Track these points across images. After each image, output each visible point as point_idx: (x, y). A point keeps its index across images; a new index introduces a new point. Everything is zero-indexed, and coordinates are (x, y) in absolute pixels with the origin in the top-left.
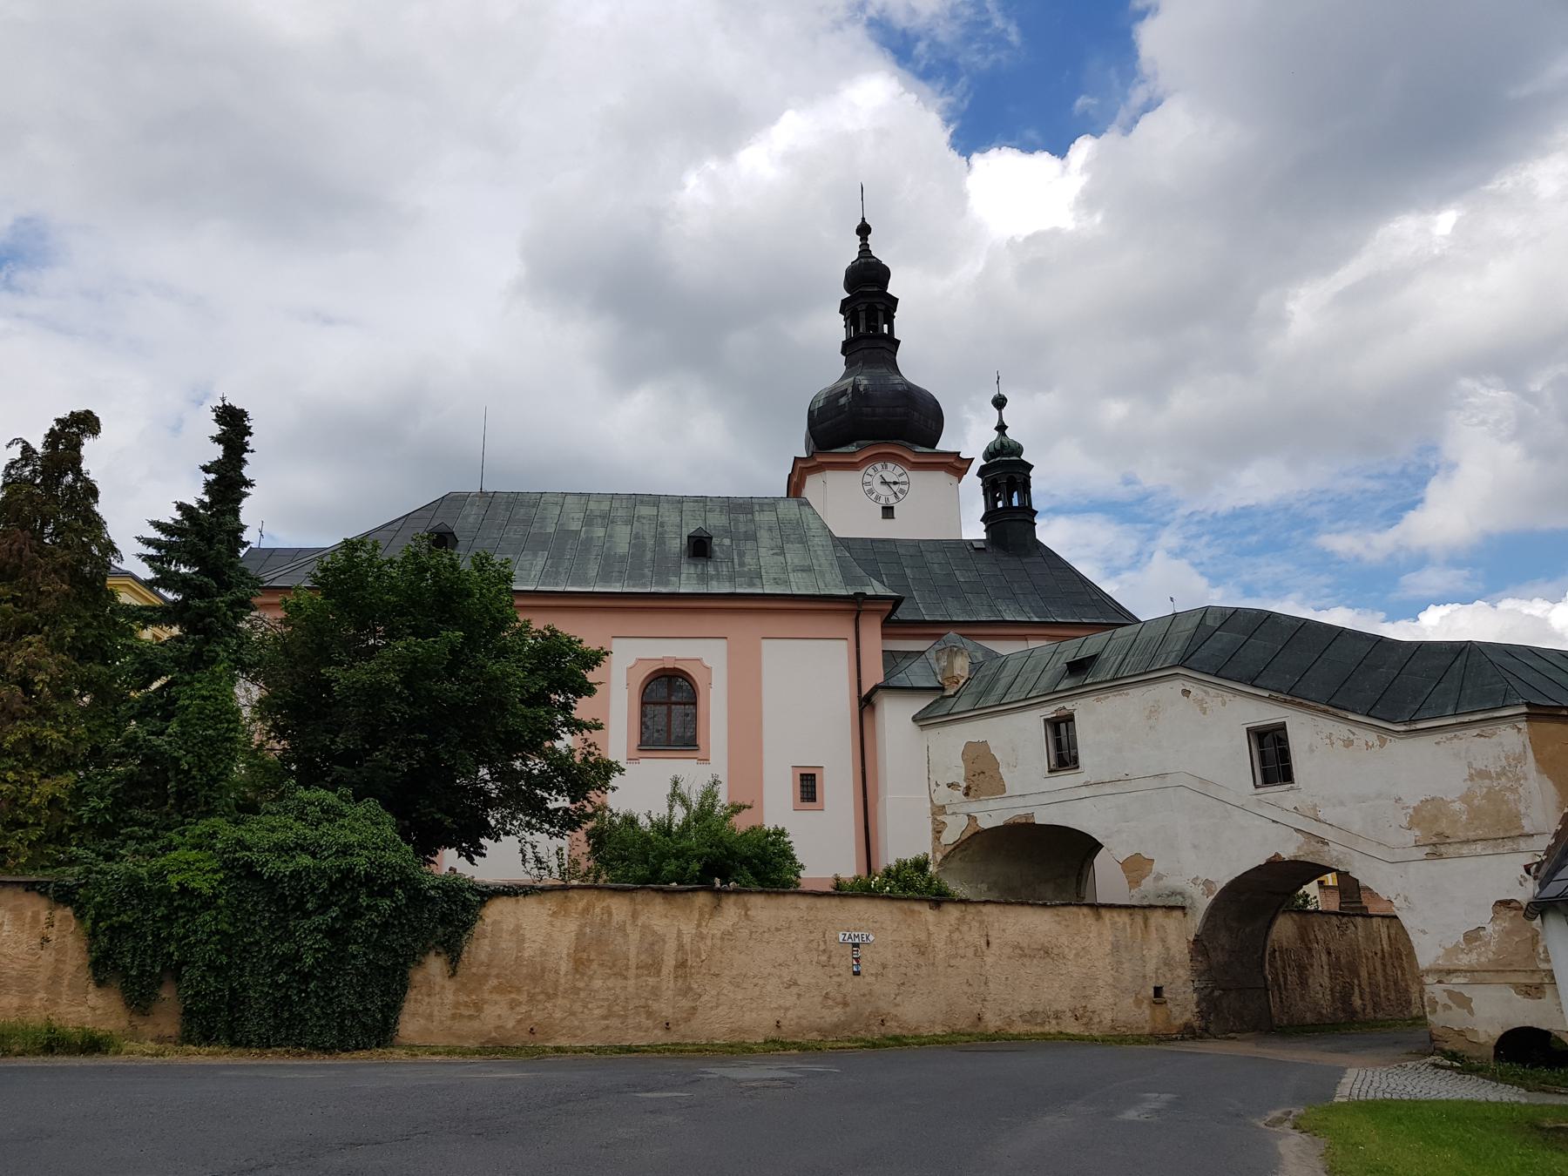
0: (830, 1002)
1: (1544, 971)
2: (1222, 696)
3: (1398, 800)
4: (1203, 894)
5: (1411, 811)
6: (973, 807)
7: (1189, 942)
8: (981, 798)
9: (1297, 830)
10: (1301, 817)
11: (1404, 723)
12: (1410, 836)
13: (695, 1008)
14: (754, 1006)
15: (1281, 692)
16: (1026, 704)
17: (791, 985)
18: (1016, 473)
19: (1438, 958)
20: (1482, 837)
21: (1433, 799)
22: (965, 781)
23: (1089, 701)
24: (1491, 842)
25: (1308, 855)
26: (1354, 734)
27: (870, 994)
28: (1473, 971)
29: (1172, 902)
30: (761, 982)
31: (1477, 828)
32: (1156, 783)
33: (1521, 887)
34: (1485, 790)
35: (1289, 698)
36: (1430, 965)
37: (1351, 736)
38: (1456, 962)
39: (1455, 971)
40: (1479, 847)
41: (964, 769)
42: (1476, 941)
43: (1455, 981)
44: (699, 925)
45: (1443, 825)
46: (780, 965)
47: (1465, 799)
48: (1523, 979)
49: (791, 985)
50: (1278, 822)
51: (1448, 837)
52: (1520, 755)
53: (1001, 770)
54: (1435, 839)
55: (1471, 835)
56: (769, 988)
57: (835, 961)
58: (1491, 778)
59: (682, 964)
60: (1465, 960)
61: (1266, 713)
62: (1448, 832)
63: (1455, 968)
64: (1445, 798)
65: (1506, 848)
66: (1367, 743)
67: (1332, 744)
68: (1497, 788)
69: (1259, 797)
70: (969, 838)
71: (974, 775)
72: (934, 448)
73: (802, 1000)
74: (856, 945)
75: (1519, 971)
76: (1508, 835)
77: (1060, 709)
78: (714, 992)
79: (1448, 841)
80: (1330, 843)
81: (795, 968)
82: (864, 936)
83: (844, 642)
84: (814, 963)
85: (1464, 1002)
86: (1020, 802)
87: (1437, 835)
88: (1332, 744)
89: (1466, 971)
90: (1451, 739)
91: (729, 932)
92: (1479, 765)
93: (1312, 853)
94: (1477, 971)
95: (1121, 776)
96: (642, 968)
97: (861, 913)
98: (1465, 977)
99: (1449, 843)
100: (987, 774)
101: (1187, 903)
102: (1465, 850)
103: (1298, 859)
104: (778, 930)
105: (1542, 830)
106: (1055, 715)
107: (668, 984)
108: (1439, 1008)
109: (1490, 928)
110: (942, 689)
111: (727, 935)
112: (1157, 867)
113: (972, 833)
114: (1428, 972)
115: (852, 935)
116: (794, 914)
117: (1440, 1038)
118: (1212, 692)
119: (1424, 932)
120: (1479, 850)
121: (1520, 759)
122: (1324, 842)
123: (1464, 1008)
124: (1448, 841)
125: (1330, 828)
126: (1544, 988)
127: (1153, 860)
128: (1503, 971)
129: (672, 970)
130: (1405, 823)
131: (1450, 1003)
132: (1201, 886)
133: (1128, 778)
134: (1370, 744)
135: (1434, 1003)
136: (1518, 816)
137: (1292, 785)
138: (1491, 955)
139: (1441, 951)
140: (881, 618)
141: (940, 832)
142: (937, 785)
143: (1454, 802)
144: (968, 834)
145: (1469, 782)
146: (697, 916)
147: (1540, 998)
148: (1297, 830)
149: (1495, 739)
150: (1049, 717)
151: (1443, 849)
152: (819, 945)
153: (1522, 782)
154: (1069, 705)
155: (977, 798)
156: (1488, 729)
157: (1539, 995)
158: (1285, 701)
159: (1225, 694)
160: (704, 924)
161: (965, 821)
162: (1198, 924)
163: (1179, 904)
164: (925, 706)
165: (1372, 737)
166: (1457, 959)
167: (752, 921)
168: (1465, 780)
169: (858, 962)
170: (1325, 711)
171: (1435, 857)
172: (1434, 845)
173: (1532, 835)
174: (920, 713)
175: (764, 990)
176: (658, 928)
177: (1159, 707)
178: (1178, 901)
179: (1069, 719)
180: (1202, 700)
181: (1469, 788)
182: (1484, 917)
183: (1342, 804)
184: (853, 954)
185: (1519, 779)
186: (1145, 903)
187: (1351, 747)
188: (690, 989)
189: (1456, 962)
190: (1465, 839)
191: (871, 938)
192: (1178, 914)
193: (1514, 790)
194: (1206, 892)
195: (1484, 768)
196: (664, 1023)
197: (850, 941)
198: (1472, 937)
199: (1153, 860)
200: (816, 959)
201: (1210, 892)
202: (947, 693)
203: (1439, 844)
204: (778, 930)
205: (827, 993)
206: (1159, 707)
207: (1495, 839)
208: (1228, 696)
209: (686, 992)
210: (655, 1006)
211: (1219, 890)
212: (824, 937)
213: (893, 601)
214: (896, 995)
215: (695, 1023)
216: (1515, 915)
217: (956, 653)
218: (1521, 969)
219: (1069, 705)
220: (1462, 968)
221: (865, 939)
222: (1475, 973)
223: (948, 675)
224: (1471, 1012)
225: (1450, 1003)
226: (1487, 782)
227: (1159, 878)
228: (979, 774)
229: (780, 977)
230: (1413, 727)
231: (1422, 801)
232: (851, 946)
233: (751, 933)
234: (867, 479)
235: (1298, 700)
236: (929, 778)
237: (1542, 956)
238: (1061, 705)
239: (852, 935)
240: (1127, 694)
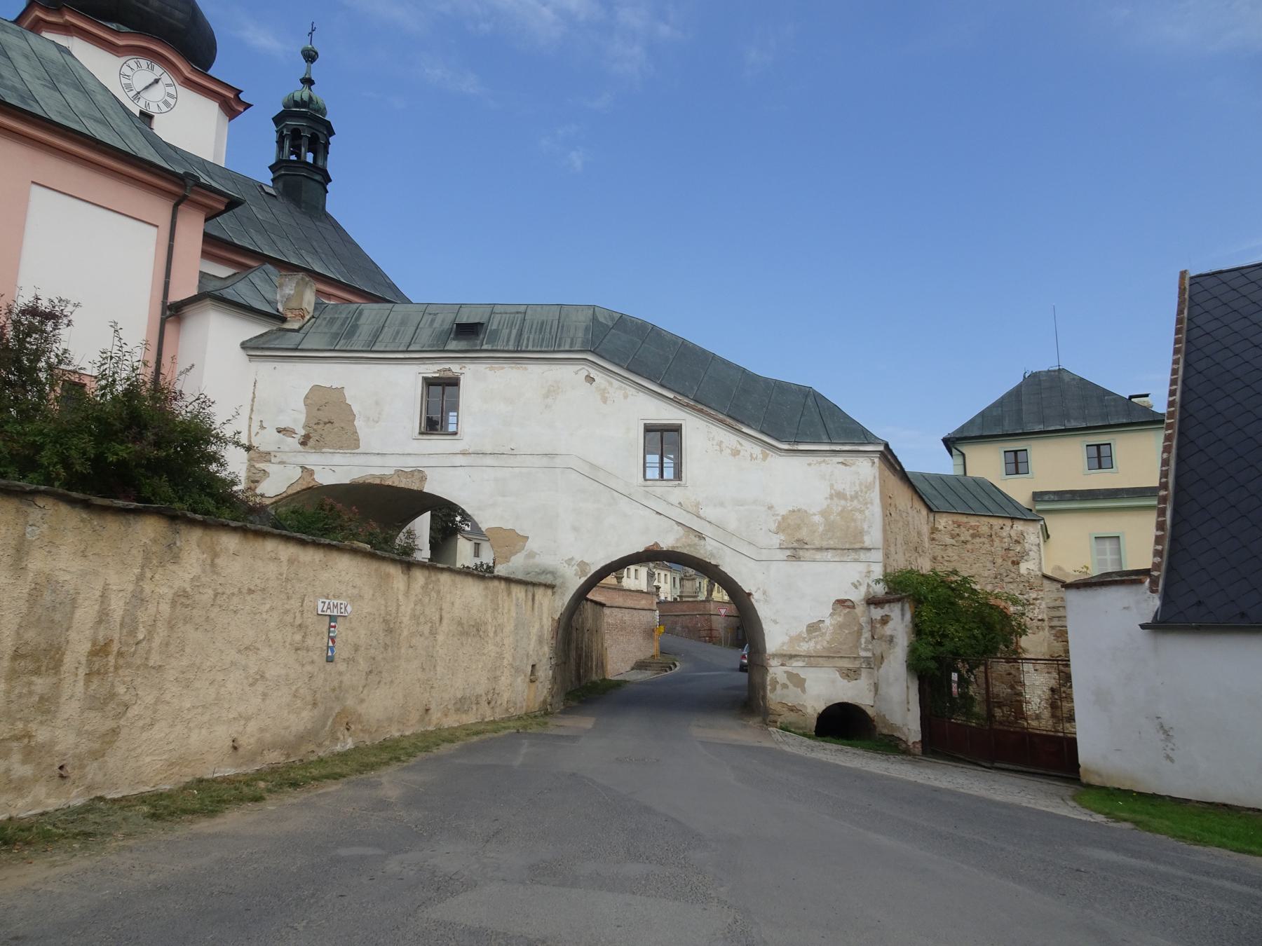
0: (299, 703)
1: (864, 658)
2: (625, 389)
3: (771, 508)
4: (575, 575)
5: (779, 518)
6: (311, 459)
7: (553, 619)
8: (324, 450)
9: (679, 524)
10: (684, 512)
11: (789, 442)
12: (776, 540)
13: (115, 732)
14: (206, 718)
15: (687, 397)
16: (405, 353)
17: (257, 680)
18: (320, 132)
19: (783, 644)
20: (832, 546)
21: (799, 510)
22: (304, 427)
23: (481, 368)
24: (839, 551)
25: (685, 547)
26: (741, 444)
27: (340, 687)
28: (810, 657)
29: (542, 579)
30: (220, 677)
31: (829, 539)
32: (545, 461)
33: (855, 590)
34: (840, 508)
35: (692, 403)
36: (776, 651)
37: (738, 446)
38: (798, 648)
39: (796, 656)
40: (829, 555)
41: (305, 415)
42: (816, 632)
43: (795, 664)
44: (141, 578)
45: (804, 534)
46: (246, 648)
47: (825, 513)
48: (846, 664)
49: (257, 680)
50: (661, 514)
51: (806, 544)
52: (870, 483)
53: (356, 423)
54: (795, 545)
55: (825, 544)
56: (230, 686)
57: (310, 642)
58: (846, 499)
59: (100, 650)
60: (804, 647)
61: (666, 413)
62: (807, 539)
63: (797, 653)
64: (808, 511)
65: (850, 557)
66: (751, 455)
67: (721, 451)
68: (850, 508)
69: (646, 489)
70: (298, 492)
71: (318, 424)
72: (206, 71)
73: (268, 702)
74: (333, 618)
75: (845, 657)
76: (852, 547)
77: (445, 370)
78: (150, 699)
79: (806, 546)
80: (707, 538)
81: (265, 652)
82: (343, 606)
83: (154, 230)
84: (287, 644)
85: (799, 682)
86: (377, 461)
87: (798, 541)
88: (721, 451)
89: (804, 656)
90: (820, 463)
91: (185, 591)
92: (839, 487)
93: (689, 545)
94: (813, 657)
95: (506, 450)
96: (23, 656)
97: (343, 573)
98: (804, 661)
99: (807, 549)
100: (336, 425)
101: (558, 582)
102: (818, 556)
103: (675, 550)
104: (251, 591)
105: (877, 547)
106: (437, 375)
107: (74, 689)
108: (778, 687)
109: (828, 622)
110: (283, 319)
111: (181, 598)
112: (531, 545)
113: (304, 487)
114: (774, 656)
115: (331, 604)
116: (272, 569)
117: (775, 713)
118: (616, 383)
119: (775, 622)
120: (829, 557)
121: (869, 487)
122: (700, 536)
123: (798, 687)
124: (806, 546)
125: (708, 525)
126: (861, 671)
127: (527, 538)
128: (833, 657)
129: (83, 660)
130: (773, 527)
131: (788, 683)
132: (575, 567)
133: (514, 452)
134: (754, 456)
135: (775, 682)
136: (862, 533)
137: (679, 482)
138: (825, 644)
139: (786, 639)
140: (206, 215)
141: (257, 482)
142: (262, 427)
143: (815, 515)
144: (298, 488)
145: (829, 501)
146: (139, 560)
147: (856, 679)
148: (679, 524)
149: (853, 468)
150: (430, 375)
151: (801, 553)
152: (295, 618)
153: (869, 506)
154: (455, 368)
155: (318, 448)
156: (849, 459)
157: (856, 677)
158: (688, 406)
159: (627, 387)
160: (149, 575)
161: (298, 473)
162: (566, 604)
163: (549, 582)
164: (252, 336)
165: (757, 450)
166: (798, 646)
167: (218, 574)
168: (827, 498)
169: (333, 642)
170: (721, 421)
171: (794, 559)
172: (795, 549)
173: (870, 549)
174: (251, 340)
175: (223, 690)
176: (67, 577)
177: (559, 388)
178: (548, 579)
179: (454, 382)
180: (605, 389)
181: (828, 505)
182: (824, 612)
183: (722, 504)
184: (329, 633)
185: (866, 504)
186: (528, 579)
187: (737, 457)
188: (112, 695)
189: (798, 648)
190: (819, 547)
191: (349, 609)
192: (549, 592)
193: (861, 512)
194: (580, 573)
195: (842, 491)
196: (56, 768)
197: (329, 613)
198: (813, 628)
199: (527, 538)
200: (289, 640)
201: (583, 572)
202: (287, 326)
203: (799, 549)
204: (251, 591)
205: (297, 690)
206: (559, 388)
207: (842, 549)
208: (631, 391)
209: (98, 703)
210: (42, 735)
211: (593, 572)
212: (302, 606)
213: (226, 201)
214: (364, 687)
215: (112, 761)
216: (848, 612)
217: (307, 283)
218: (846, 656)
219: (455, 368)
220: (802, 654)
221: (343, 610)
222: (812, 659)
223: (293, 304)
224: (804, 691)
225: (788, 683)
226: (843, 502)
227: (531, 555)
228: (325, 423)
229: (245, 668)
230: (795, 447)
231: (790, 511)
232: (328, 618)
233: (216, 595)
234: (126, 70)
235: (700, 406)
236: (250, 418)
237: (863, 646)
238: (447, 366)
239: (331, 604)
240: (526, 369)
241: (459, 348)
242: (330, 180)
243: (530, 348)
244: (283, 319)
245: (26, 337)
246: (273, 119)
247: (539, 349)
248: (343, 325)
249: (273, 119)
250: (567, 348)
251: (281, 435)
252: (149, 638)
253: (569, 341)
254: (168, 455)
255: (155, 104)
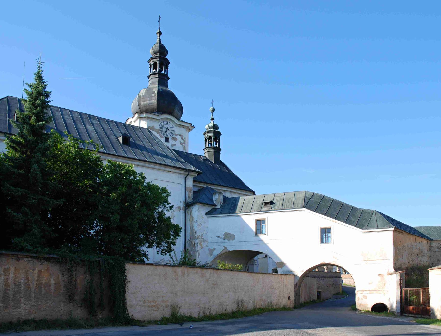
22: (224, 236)
85: (365, 297)
121: (184, 148)
241: (265, 210)
242: (221, 150)
243: (285, 208)
244: (216, 205)
245: (53, 166)
246: (221, 134)
247: (288, 208)
248: (232, 205)
249: (221, 134)
250: (296, 207)
251: (218, 238)
252: (58, 202)
253: (297, 205)
254: (80, 183)
255: (172, 128)
